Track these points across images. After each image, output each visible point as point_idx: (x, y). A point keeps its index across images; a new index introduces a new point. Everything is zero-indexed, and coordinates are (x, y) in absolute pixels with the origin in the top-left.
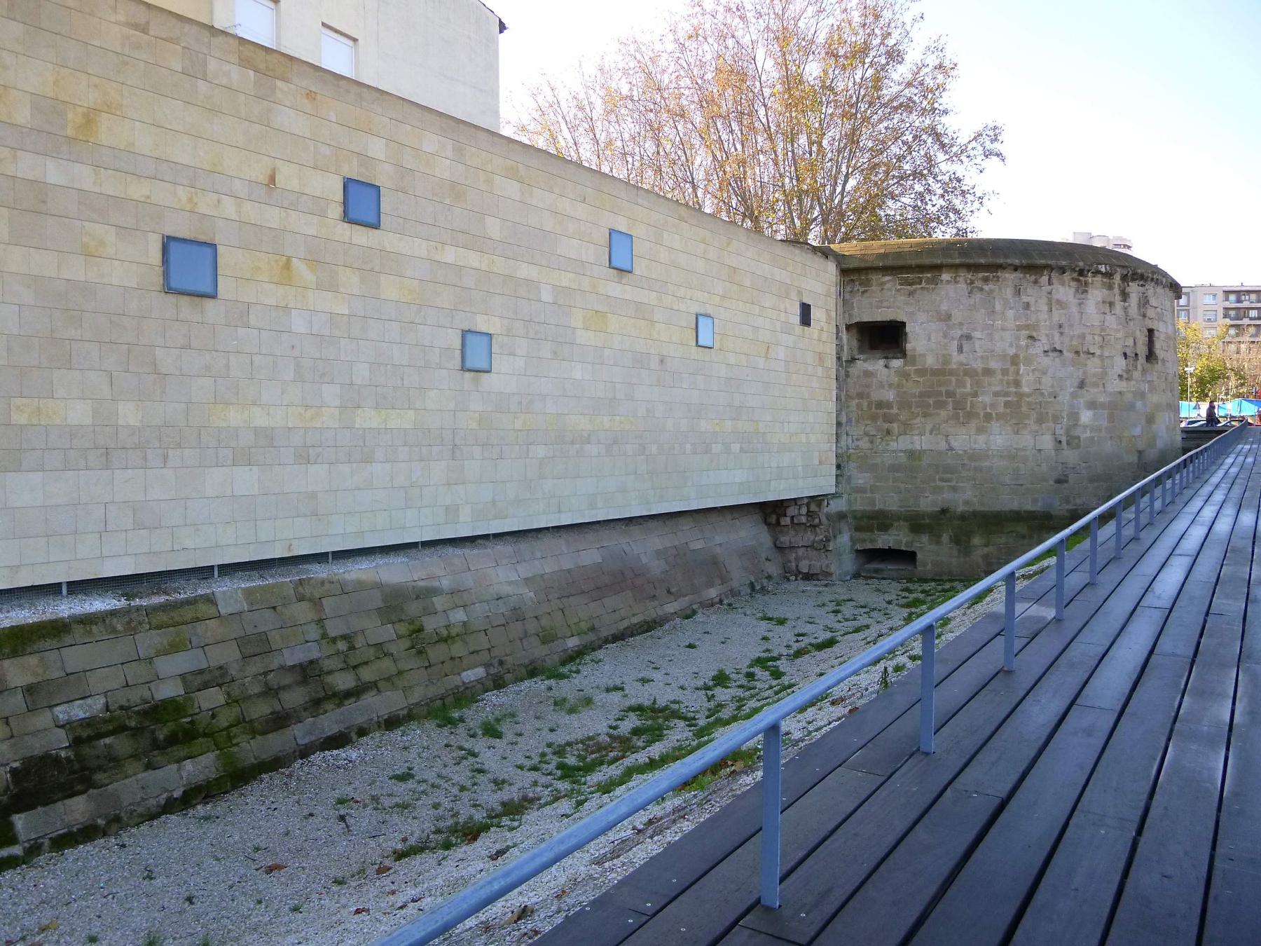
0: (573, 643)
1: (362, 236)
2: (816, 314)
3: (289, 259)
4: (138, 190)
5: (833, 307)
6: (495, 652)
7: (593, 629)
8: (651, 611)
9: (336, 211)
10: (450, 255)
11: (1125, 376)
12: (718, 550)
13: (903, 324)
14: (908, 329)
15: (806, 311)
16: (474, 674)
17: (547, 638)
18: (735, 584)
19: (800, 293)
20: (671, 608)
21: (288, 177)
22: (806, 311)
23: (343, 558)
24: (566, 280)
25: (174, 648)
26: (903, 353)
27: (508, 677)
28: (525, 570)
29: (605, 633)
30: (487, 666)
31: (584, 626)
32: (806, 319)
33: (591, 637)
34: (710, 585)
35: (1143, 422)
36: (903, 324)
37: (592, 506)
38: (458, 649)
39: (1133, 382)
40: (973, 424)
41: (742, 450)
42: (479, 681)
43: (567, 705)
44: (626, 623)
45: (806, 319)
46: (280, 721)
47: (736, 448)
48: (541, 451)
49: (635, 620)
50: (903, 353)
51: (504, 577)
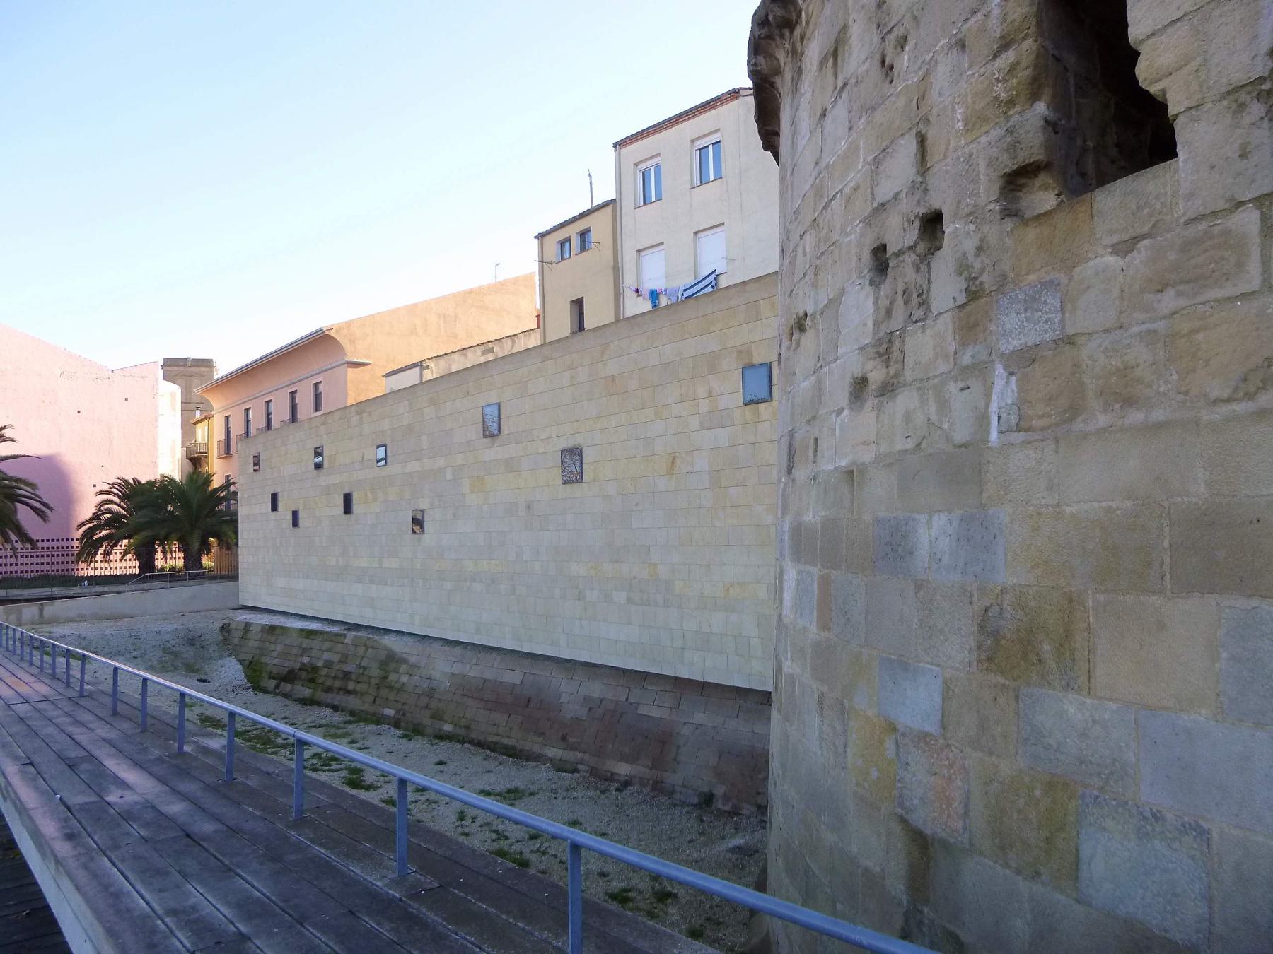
0: (448, 728)
6: (406, 707)
7: (467, 727)
8: (531, 744)
11: (877, 376)
12: (686, 731)
16: (389, 712)
17: (437, 716)
18: (674, 779)
20: (551, 752)
24: (459, 459)
25: (329, 650)
27: (403, 724)
28: (457, 669)
29: (473, 735)
30: (397, 712)
31: (463, 723)
33: (462, 732)
34: (624, 759)
35: (957, 649)
37: (478, 631)
38: (392, 696)
39: (905, 400)
41: (629, 600)
42: (389, 717)
44: (496, 739)
46: (329, 690)
47: (621, 597)
48: (448, 585)
49: (506, 741)
51: (441, 668)
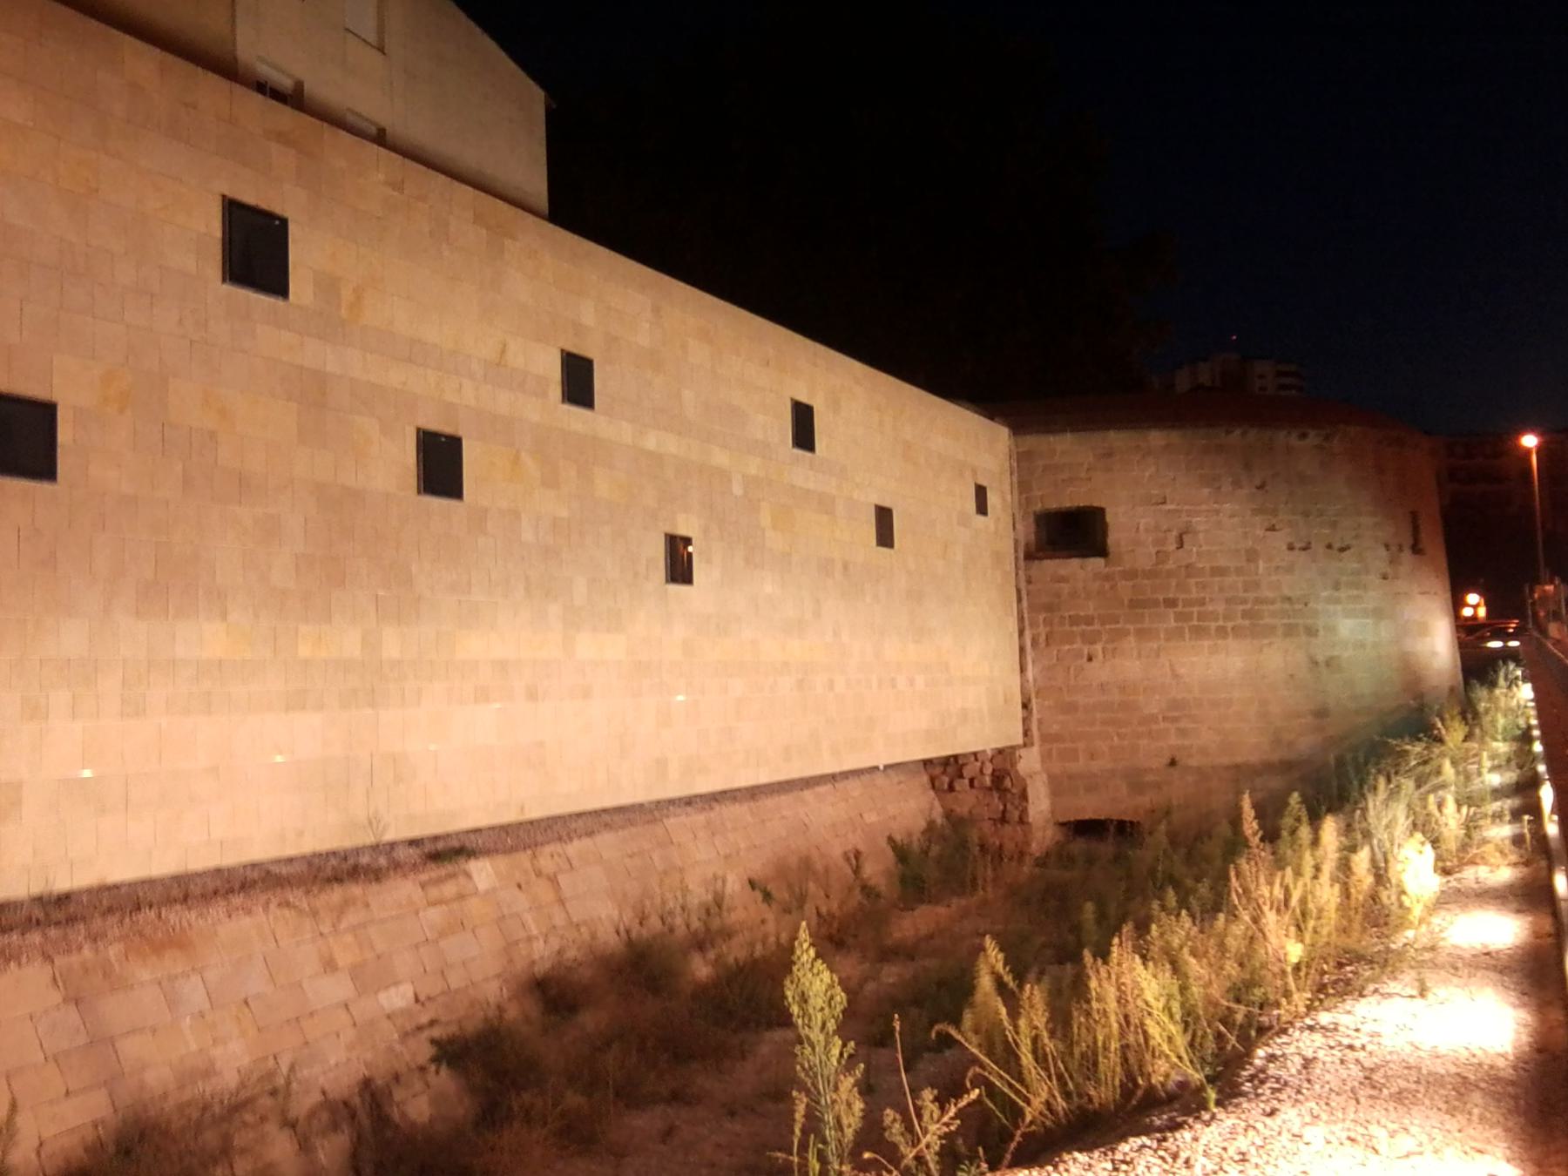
1: (575, 416)
2: (993, 499)
3: (518, 451)
4: (396, 376)
5: (1007, 487)
9: (556, 391)
10: (651, 442)
13: (1101, 511)
14: (1109, 518)
15: (981, 492)
19: (974, 472)
21: (516, 358)
22: (981, 492)
23: (505, 829)
26: (1101, 551)
32: (982, 509)
36: (1101, 511)
40: (1454, 734)
43: (222, 891)
45: (982, 509)
50: (1101, 551)
